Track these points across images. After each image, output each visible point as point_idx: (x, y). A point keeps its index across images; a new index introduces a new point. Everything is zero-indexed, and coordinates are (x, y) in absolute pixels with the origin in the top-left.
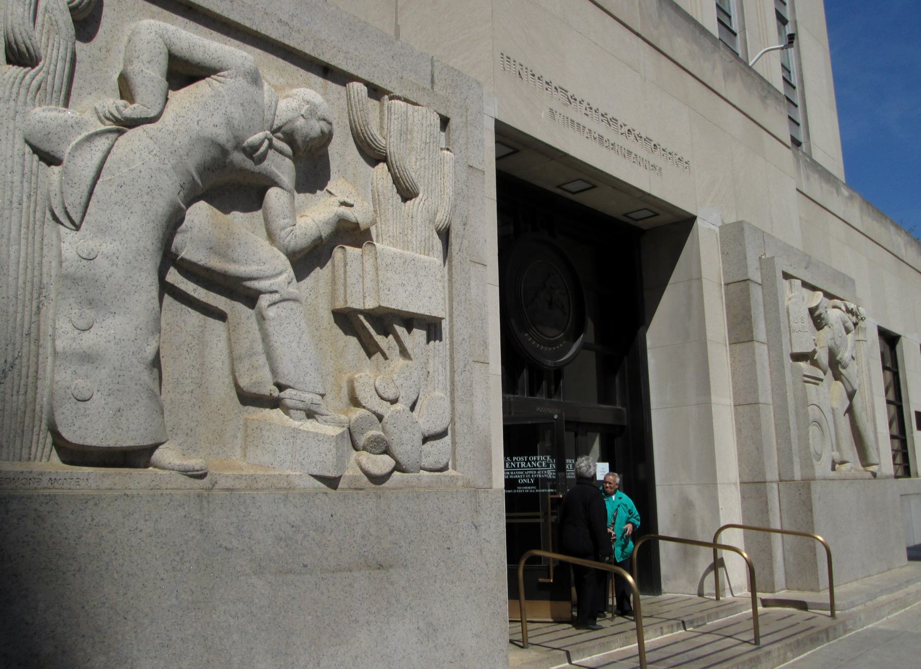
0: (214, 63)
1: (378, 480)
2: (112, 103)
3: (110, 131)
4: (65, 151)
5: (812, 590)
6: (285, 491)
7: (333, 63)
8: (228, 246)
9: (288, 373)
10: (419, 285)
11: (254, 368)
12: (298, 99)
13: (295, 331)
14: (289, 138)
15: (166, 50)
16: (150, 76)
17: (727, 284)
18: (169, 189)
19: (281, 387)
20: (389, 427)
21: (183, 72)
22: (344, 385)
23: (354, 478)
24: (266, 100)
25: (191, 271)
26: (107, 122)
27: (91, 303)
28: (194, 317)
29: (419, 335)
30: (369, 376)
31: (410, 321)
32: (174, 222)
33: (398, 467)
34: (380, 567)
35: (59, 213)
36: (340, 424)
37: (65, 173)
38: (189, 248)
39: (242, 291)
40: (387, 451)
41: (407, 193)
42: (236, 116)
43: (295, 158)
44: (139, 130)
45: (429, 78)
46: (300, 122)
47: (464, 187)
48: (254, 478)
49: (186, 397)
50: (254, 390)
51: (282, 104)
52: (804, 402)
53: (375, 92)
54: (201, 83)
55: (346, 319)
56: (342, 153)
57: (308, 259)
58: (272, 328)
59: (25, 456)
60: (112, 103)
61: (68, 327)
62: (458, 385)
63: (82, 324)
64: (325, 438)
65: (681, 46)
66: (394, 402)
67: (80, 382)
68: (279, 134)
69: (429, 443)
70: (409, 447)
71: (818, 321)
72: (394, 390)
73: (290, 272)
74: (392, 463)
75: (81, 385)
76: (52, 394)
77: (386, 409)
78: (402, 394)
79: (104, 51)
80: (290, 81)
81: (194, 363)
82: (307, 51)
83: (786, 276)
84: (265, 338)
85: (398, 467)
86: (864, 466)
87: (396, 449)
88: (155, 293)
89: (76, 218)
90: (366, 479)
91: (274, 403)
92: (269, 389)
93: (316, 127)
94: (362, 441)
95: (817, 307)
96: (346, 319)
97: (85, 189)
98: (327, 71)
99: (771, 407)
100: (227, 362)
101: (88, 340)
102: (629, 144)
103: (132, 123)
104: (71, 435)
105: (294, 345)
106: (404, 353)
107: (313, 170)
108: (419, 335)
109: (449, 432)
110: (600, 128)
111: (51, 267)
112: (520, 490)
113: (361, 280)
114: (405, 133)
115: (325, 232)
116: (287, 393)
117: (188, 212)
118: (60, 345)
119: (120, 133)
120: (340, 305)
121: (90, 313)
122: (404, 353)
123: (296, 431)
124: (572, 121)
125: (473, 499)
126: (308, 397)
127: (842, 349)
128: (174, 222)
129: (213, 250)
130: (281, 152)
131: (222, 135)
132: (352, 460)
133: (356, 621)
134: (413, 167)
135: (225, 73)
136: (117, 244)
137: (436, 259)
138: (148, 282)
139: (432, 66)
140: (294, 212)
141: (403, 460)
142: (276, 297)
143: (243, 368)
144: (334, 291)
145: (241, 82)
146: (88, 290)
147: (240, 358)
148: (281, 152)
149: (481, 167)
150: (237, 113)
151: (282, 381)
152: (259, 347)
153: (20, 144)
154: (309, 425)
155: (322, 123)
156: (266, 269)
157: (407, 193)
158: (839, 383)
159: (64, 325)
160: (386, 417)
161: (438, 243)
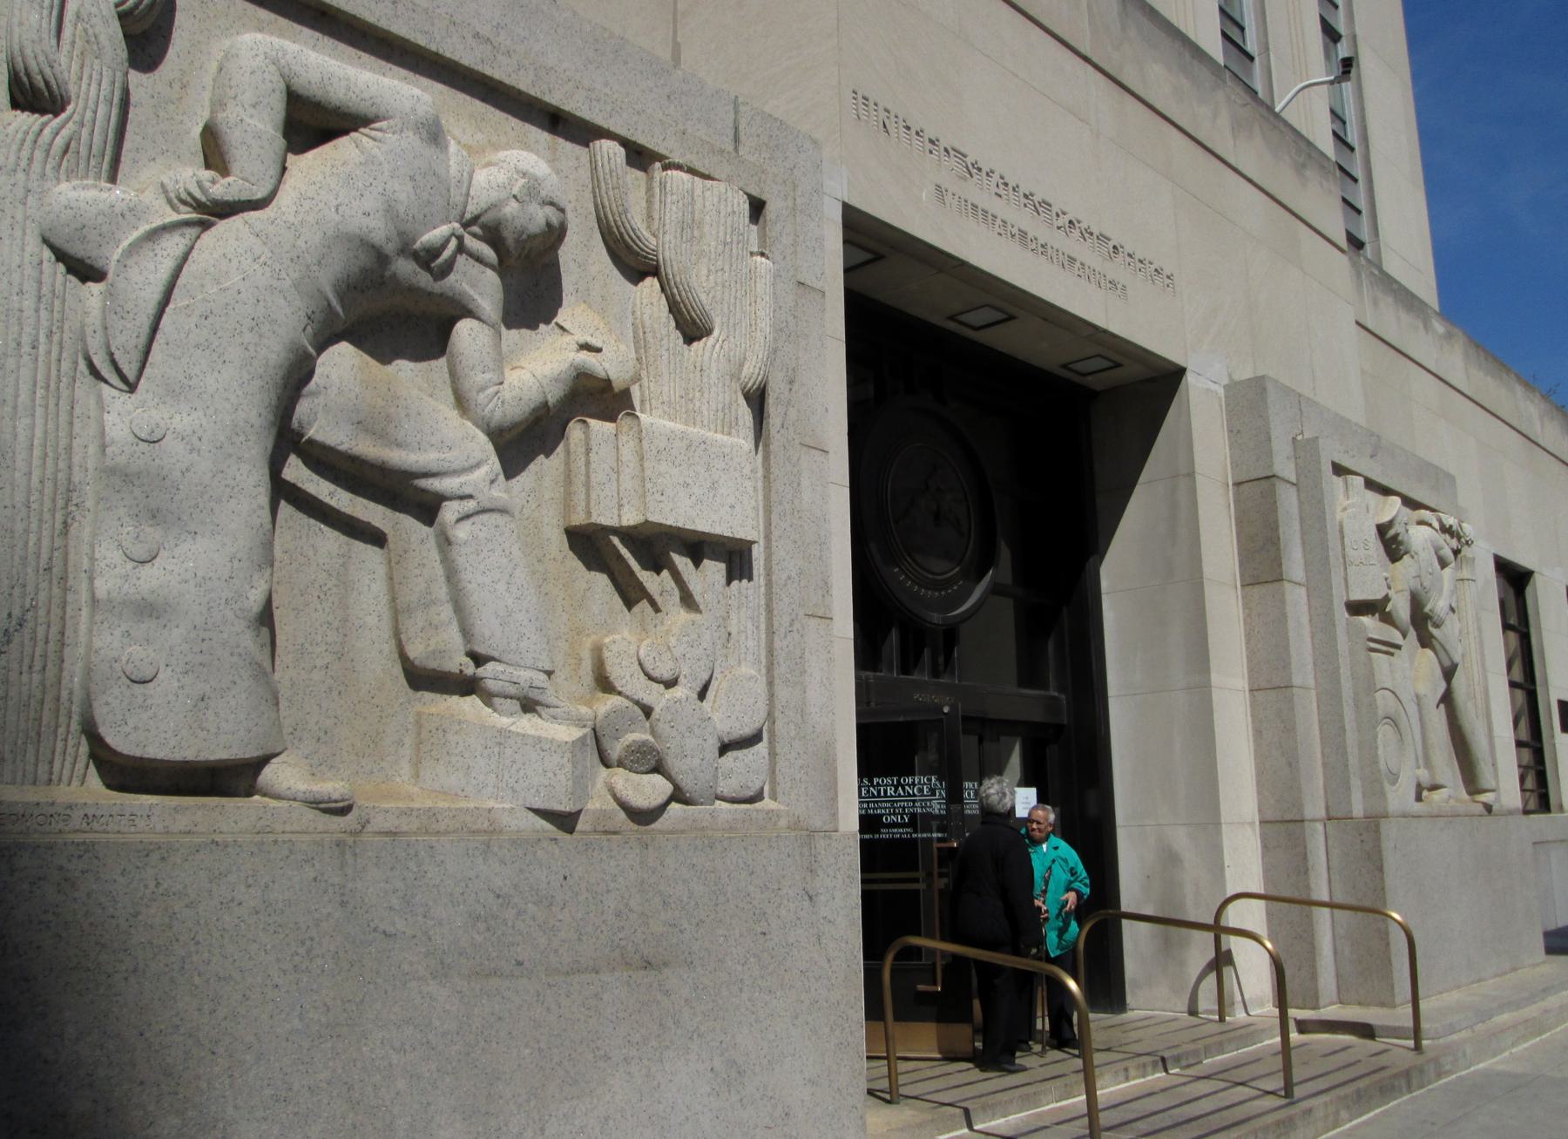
0: (364, 108)
1: (643, 817)
2: (191, 176)
3: (187, 224)
4: (111, 257)
5: (1382, 1005)
6: (485, 836)
7: (566, 108)
8: (389, 419)
9: (490, 635)
10: (714, 486)
11: (433, 626)
12: (507, 168)
13: (503, 563)
14: (493, 235)
15: (282, 86)
16: (255, 129)
17: (1237, 484)
18: (287, 322)
19: (479, 659)
20: (662, 727)
21: (311, 123)
22: (586, 655)
23: (603, 814)
24: (453, 170)
25: (326, 461)
26: (183, 208)
27: (154, 516)
28: (330, 540)
29: (714, 570)
30: (628, 641)
31: (698, 547)
32: (296, 378)
33: (678, 796)
34: (647, 965)
35: (100, 362)
36: (579, 722)
37: (110, 294)
38: (323, 422)
39: (413, 496)
40: (658, 769)
41: (692, 329)
42: (402, 197)
43: (502, 268)
44: (236, 222)
45: (731, 133)
46: (511, 208)
47: (790, 319)
48: (433, 814)
49: (317, 676)
50: (433, 664)
51: (481, 177)
52: (1369, 685)
53: (639, 156)
54: (343, 141)
55: (589, 544)
56: (583, 260)
57: (525, 440)
58: (463, 558)
59: (43, 776)
60: (191, 176)
61: (116, 556)
62: (780, 656)
63: (140, 551)
64: (553, 746)
65: (1159, 78)
66: (671, 684)
67: (136, 651)
68: (476, 229)
69: (731, 755)
70: (697, 761)
71: (1393, 547)
72: (671, 664)
73: (494, 464)
74: (668, 788)
75: (139, 655)
76: (88, 671)
77: (657, 697)
78: (685, 670)
79: (176, 86)
80: (494, 139)
81: (330, 618)
82: (523, 87)
83: (1339, 470)
84: (452, 575)
85: (678, 796)
86: (1470, 793)
87: (674, 764)
88: (264, 499)
89: (130, 371)
90: (622, 815)
91: (467, 686)
92: (458, 662)
93: (539, 217)
94: (616, 750)
95: (1391, 523)
96: (589, 544)
97: (145, 322)
98: (557, 122)
99: (1313, 693)
100: (387, 616)
101: (150, 579)
102: (1071, 244)
103: (225, 210)
104: (121, 740)
105: (501, 587)
106: (688, 600)
107: (533, 289)
108: (714, 570)
109: (765, 735)
110: (1022, 218)
111: (86, 454)
112: (885, 834)
113: (614, 476)
114: (690, 226)
115: (554, 395)
116: (488, 670)
117: (319, 361)
118: (102, 587)
119: (205, 226)
120: (578, 519)
121: (153, 533)
122: (688, 600)
123: (504, 733)
124: (975, 206)
125: (805, 850)
126: (524, 676)
127: (1433, 594)
128: (296, 378)
129: (362, 425)
130: (479, 259)
131: (379, 230)
132: (600, 784)
133: (607, 1058)
134: (704, 285)
135: (383, 124)
136: (199, 415)
137: (743, 440)
138: (252, 480)
139: (736, 112)
140: (500, 360)
141: (687, 783)
142: (470, 505)
143: (413, 626)
144: (568, 496)
145: (411, 140)
146: (150, 494)
147: (409, 610)
148: (479, 259)
149: (818, 285)
150: (403, 193)
151: (481, 649)
152: (441, 591)
153: (33, 245)
154: (527, 724)
155: (549, 210)
156: (453, 458)
157: (692, 329)
158: (1428, 652)
159: (108, 554)
160: (657, 710)
161: (745, 414)
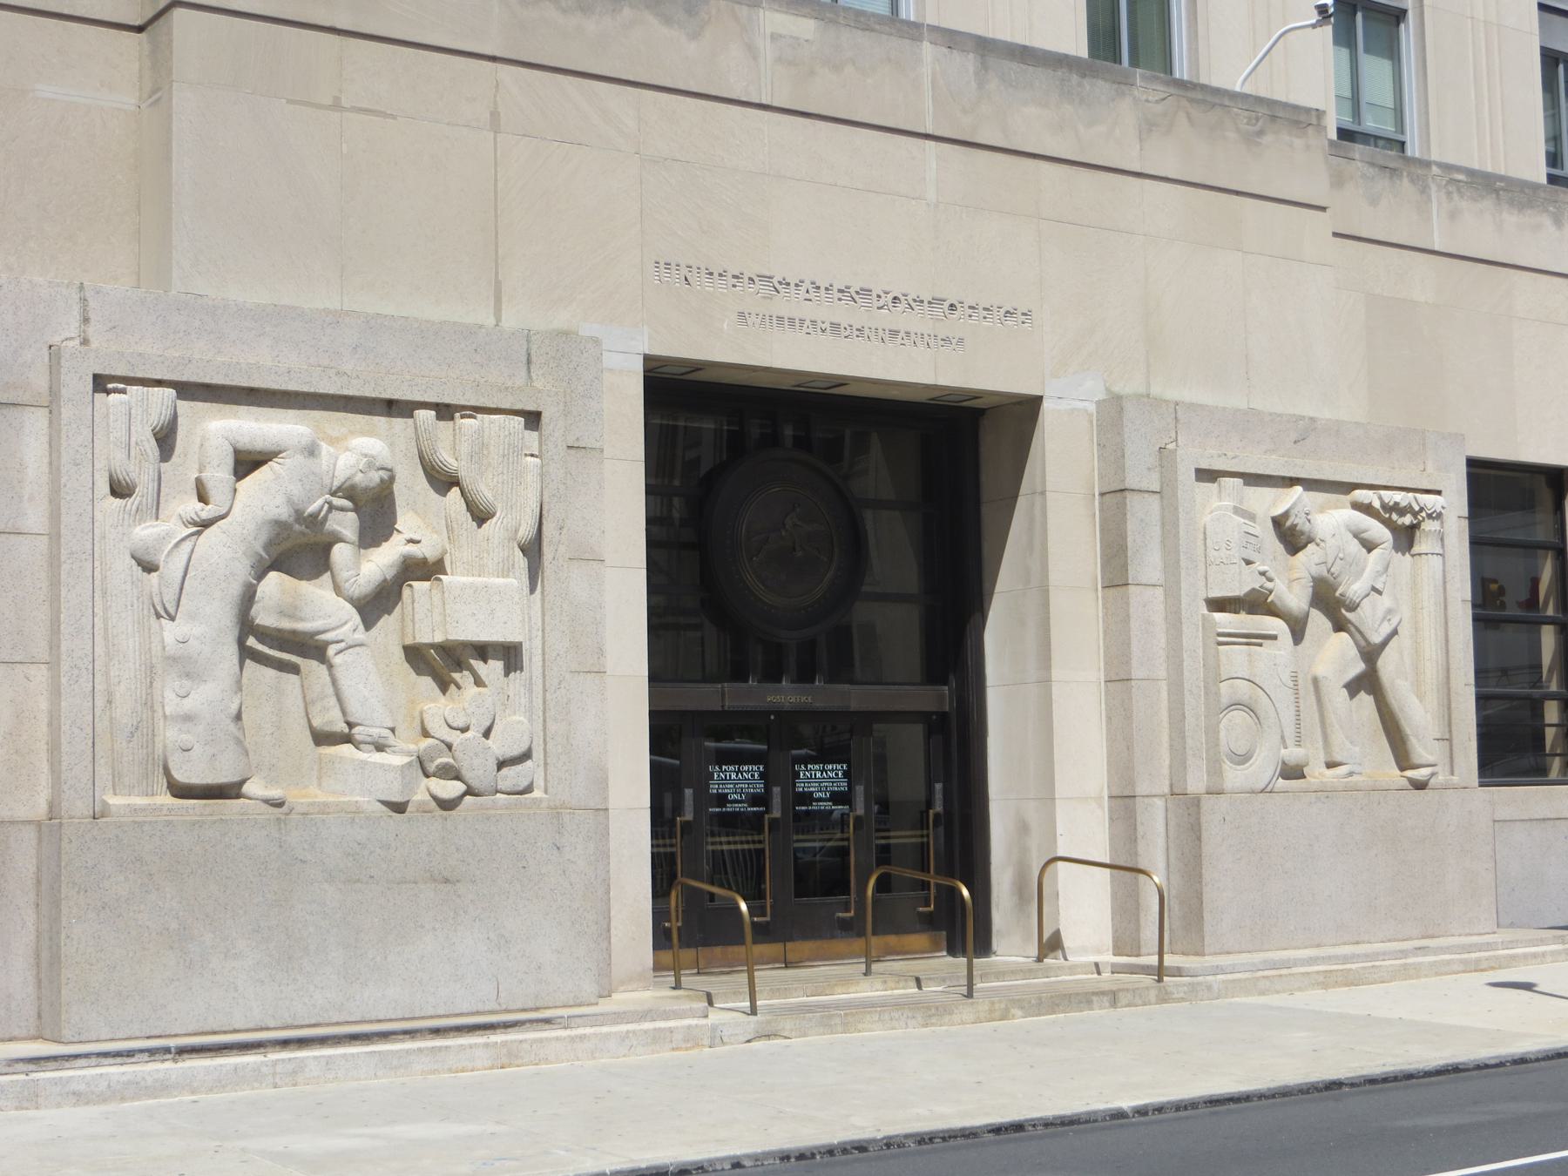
0: (274, 448)
1: (447, 805)
2: (193, 507)
3: (192, 534)
4: (161, 559)
5: (1197, 954)
6: (354, 813)
8: (296, 608)
9: (356, 713)
11: (326, 709)
12: (359, 449)
13: (367, 673)
16: (219, 474)
17: (1102, 494)
18: (242, 571)
19: (350, 725)
20: (457, 754)
21: (247, 463)
22: (417, 714)
23: (422, 803)
24: (324, 467)
25: (264, 635)
27: (187, 675)
28: (270, 673)
29: (496, 666)
30: (439, 708)
31: (483, 651)
32: (248, 598)
33: (470, 791)
34: (447, 881)
35: (159, 608)
36: (409, 754)
37: (161, 577)
38: (264, 616)
39: (310, 647)
40: (458, 778)
41: (480, 516)
42: (295, 492)
43: (356, 510)
44: (214, 527)
45: (524, 359)
46: (359, 478)
47: (562, 487)
48: (326, 804)
49: (268, 738)
50: (327, 729)
51: (341, 463)
52: (1214, 677)
53: (445, 411)
54: (265, 468)
55: (416, 656)
56: (411, 488)
57: (376, 604)
58: (340, 673)
60: (193, 507)
65: (1032, 118)
66: (464, 730)
67: (184, 737)
69: (505, 771)
71: (1291, 537)
73: (357, 618)
75: (186, 738)
76: (165, 747)
77: (455, 738)
78: (474, 721)
82: (367, 394)
83: (1207, 475)
84: (334, 682)
85: (470, 791)
86: (1402, 769)
87: (467, 774)
88: (236, 660)
89: (172, 610)
90: (434, 804)
91: (347, 739)
92: (341, 727)
93: (375, 477)
94: (432, 768)
95: (1286, 515)
96: (416, 656)
97: (177, 587)
98: (393, 408)
99: (1164, 686)
100: (302, 705)
101: (188, 705)
102: (900, 319)
103: (206, 524)
104: (181, 776)
105: (361, 686)
106: (479, 682)
107: (375, 510)
108: (496, 666)
109: (538, 754)
110: (842, 313)
111: (156, 648)
112: (729, 808)
113: (429, 615)
114: (480, 450)
115: (390, 575)
116: (355, 730)
117: (259, 590)
118: (168, 711)
119: (199, 533)
120: (409, 641)
121: (187, 683)
122: (479, 682)
123: (364, 763)
124: (780, 318)
126: (375, 732)
127: (1344, 579)
128: (248, 598)
129: (282, 613)
130: (342, 509)
131: (284, 513)
132: (423, 786)
133: (422, 927)
134: (485, 491)
136: (205, 626)
137: (517, 581)
138: (231, 651)
139: (528, 341)
140: (357, 564)
141: (475, 784)
142: (343, 645)
143: (314, 711)
144: (403, 628)
145: (299, 458)
146: (187, 667)
147: (313, 702)
148: (342, 509)
149: (598, 445)
150: (296, 490)
151: (351, 719)
152: (330, 690)
153: (128, 557)
154: (378, 757)
155: (381, 473)
156: (332, 622)
157: (480, 516)
158: (1344, 635)
159: (170, 695)
161: (521, 562)
